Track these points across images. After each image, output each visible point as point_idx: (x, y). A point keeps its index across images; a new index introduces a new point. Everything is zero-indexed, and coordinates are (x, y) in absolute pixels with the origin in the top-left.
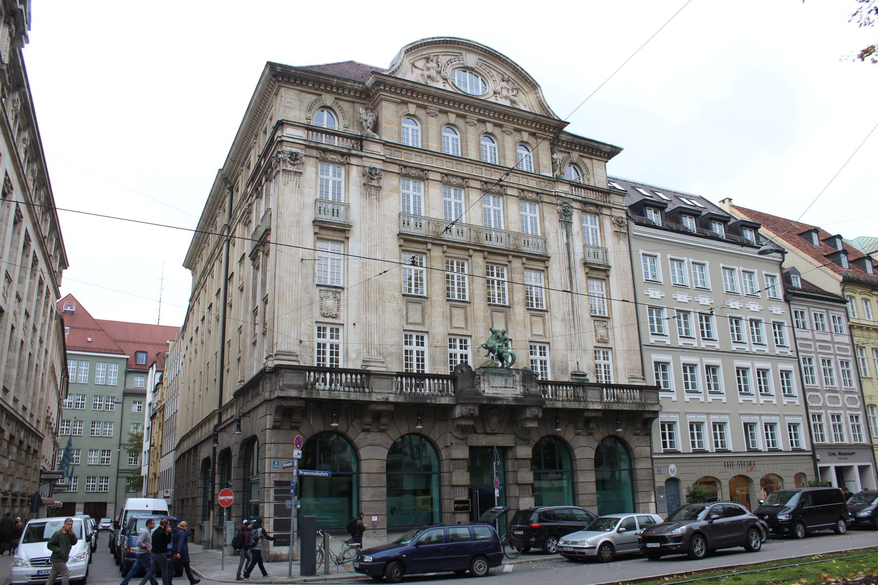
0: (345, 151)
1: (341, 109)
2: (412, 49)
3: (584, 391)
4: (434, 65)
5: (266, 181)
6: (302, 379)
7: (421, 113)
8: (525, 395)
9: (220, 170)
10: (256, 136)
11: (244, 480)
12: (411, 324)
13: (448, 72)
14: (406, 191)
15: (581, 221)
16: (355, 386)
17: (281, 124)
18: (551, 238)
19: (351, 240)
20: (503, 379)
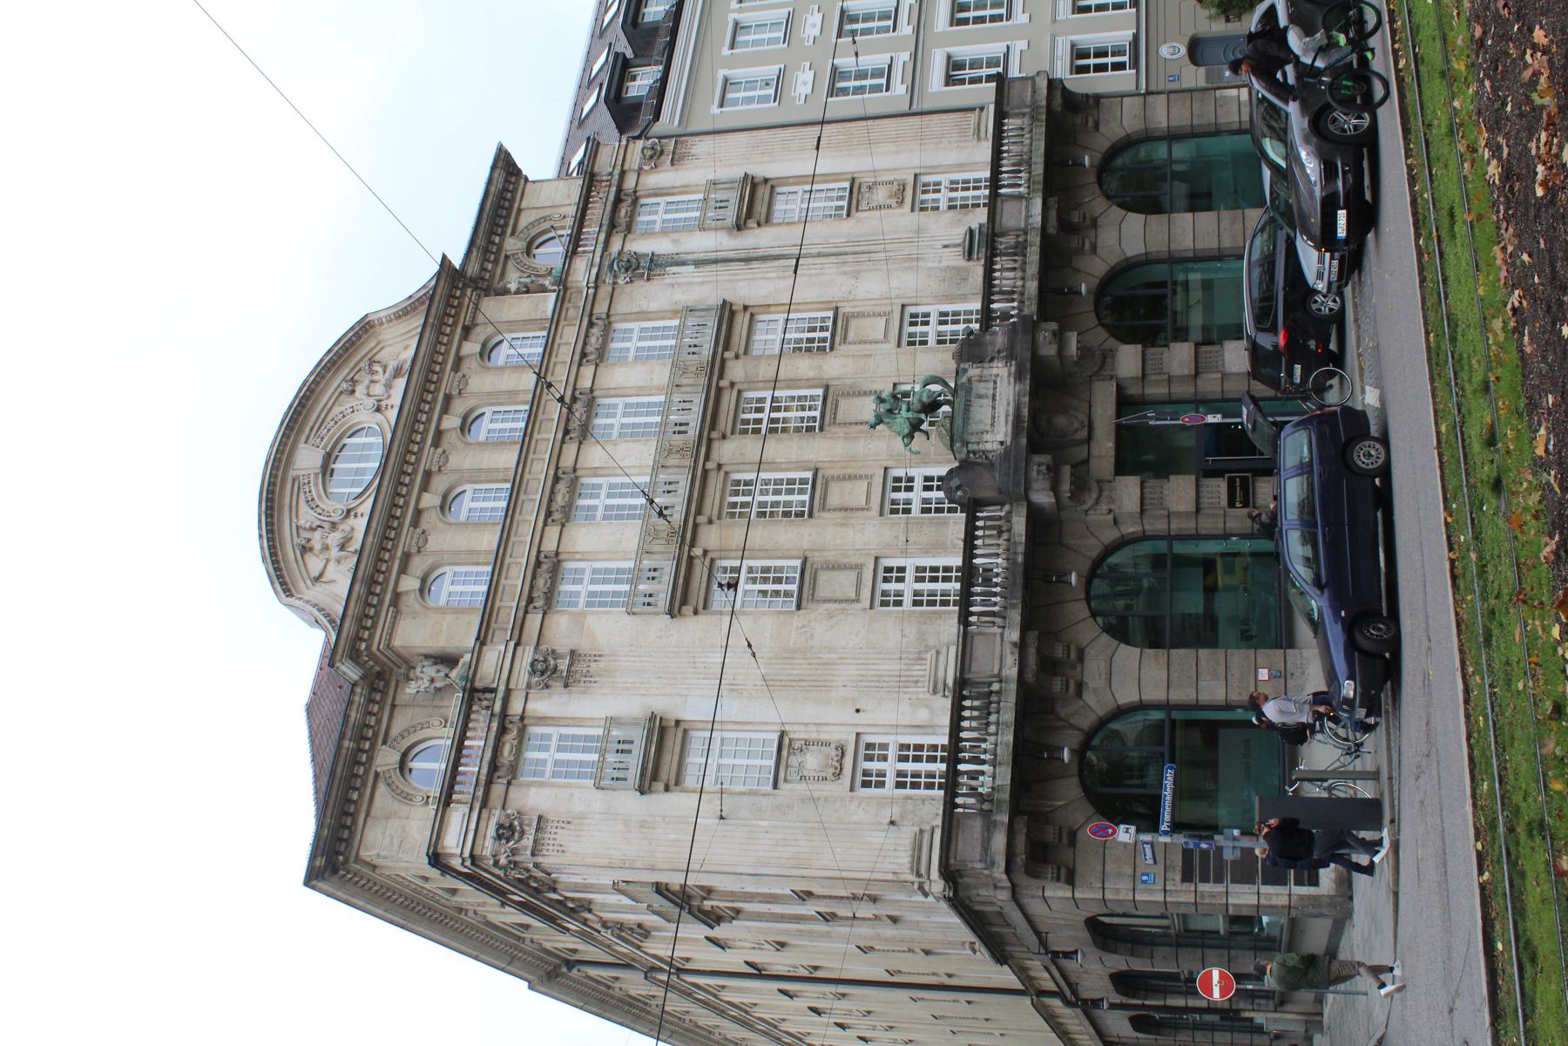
0: (495, 725)
2: (283, 581)
3: (1004, 234)
4: (317, 535)
5: (554, 890)
6: (970, 822)
9: (531, 987)
10: (460, 910)
11: (1179, 945)
13: (334, 507)
15: (649, 234)
16: (986, 711)
17: (436, 859)
18: (683, 297)
19: (681, 716)
20: (976, 402)
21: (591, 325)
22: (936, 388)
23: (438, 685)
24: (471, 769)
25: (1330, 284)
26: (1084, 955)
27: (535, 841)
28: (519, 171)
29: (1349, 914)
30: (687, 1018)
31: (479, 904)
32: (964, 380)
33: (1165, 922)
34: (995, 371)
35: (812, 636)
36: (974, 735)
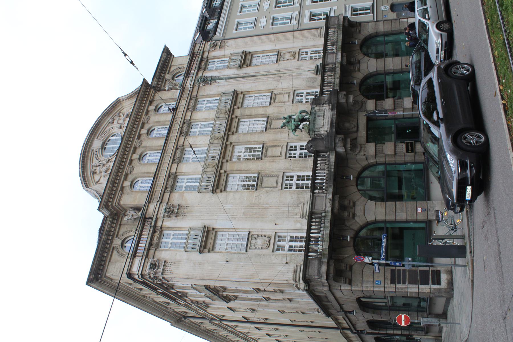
0: (152, 230)
1: (124, 233)
2: (85, 183)
3: (328, 65)
4: (98, 168)
5: (173, 289)
6: (313, 262)
7: (130, 177)
8: (329, 102)
9: (171, 325)
10: (144, 296)
11: (390, 310)
12: (277, 184)
13: (104, 159)
14: (183, 188)
15: (212, 70)
16: (320, 223)
17: (130, 275)
18: (221, 90)
19: (215, 227)
20: (317, 118)
21: (191, 99)
22: (304, 114)
23: (135, 217)
24: (143, 245)
25: (441, 61)
26: (356, 312)
27: (163, 269)
28: (171, 54)
29: (452, 296)
30: (228, 337)
31: (150, 294)
32: (314, 111)
33: (385, 301)
34: (324, 108)
35: (261, 199)
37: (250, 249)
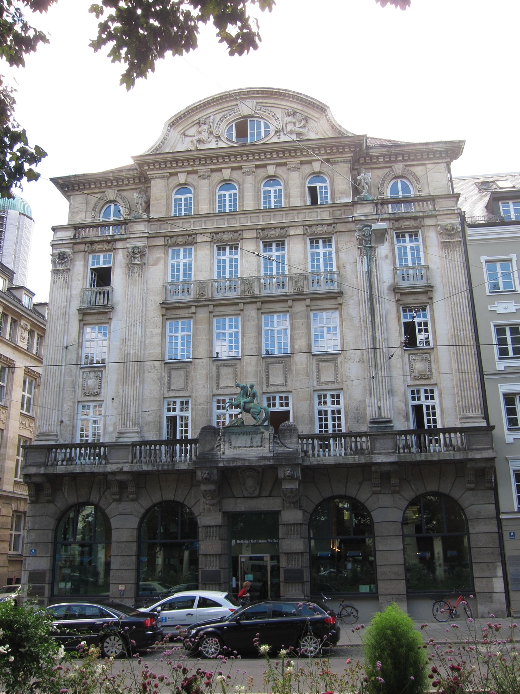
32: (262, 430)
34: (267, 446)
35: (150, 372)
36: (102, 453)
37: (409, 355)
